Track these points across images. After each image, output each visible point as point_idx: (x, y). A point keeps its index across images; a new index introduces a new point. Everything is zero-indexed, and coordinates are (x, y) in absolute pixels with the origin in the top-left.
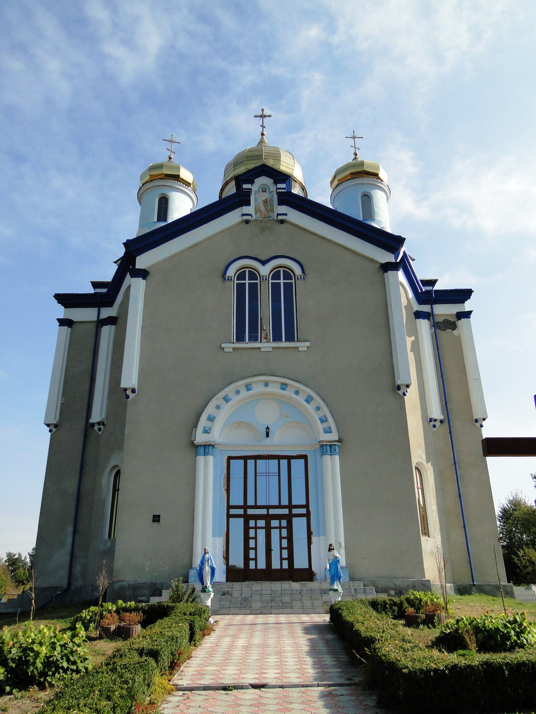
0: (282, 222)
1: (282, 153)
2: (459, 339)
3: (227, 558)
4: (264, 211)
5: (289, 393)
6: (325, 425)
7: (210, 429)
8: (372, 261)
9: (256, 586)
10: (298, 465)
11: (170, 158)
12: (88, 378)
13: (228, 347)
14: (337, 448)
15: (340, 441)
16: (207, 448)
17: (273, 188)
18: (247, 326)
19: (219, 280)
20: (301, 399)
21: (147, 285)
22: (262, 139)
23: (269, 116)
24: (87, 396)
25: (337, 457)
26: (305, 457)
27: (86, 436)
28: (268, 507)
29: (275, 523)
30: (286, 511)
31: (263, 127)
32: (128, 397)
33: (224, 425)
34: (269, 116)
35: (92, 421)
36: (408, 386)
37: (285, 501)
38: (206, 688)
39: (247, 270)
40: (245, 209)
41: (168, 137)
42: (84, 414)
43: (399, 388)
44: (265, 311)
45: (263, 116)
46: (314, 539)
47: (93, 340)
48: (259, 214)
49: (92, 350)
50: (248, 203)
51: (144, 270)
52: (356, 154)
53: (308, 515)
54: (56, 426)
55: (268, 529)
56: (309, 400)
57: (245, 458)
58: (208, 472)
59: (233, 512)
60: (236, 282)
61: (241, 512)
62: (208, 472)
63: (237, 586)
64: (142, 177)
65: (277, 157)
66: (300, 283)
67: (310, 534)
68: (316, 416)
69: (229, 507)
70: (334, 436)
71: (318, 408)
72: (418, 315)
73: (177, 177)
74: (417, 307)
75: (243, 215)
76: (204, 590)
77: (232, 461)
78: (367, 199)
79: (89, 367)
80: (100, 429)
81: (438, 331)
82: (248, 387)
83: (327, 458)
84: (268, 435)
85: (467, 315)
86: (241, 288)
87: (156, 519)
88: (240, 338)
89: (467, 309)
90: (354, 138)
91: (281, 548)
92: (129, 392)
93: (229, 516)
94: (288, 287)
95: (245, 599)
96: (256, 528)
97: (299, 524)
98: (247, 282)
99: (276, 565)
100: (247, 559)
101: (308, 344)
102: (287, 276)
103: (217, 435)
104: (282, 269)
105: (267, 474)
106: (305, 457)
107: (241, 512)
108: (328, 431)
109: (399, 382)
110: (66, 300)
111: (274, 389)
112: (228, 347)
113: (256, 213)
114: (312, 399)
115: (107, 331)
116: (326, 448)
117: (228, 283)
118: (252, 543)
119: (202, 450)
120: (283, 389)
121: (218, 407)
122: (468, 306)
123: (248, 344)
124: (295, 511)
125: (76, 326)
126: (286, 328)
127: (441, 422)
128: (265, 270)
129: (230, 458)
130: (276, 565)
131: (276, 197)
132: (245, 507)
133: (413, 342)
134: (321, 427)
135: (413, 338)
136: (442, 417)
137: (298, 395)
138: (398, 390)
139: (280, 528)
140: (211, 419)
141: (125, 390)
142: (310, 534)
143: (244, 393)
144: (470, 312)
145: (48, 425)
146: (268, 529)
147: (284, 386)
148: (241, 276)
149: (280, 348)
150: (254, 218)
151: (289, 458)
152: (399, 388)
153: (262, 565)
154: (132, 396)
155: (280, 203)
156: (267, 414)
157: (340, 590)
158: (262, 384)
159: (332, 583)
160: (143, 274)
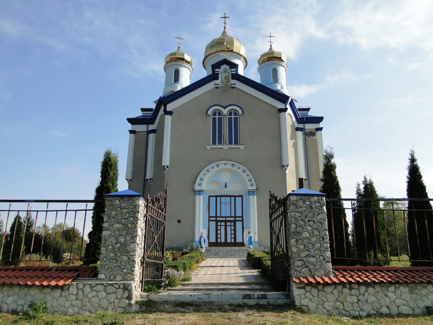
0: (233, 88)
1: (234, 39)
2: (316, 141)
3: (208, 238)
4: (225, 82)
5: (235, 168)
6: (251, 182)
7: (201, 184)
8: (275, 107)
9: (221, 248)
10: (239, 200)
11: (179, 48)
12: (144, 158)
13: (209, 147)
14: (256, 193)
15: (257, 189)
16: (200, 192)
17: (229, 71)
18: (217, 138)
19: (205, 116)
20: (240, 171)
21: (172, 119)
22: (225, 30)
23: (228, 17)
24: (144, 167)
25: (255, 197)
26: (242, 196)
27: (144, 185)
28: (226, 217)
29: (228, 224)
30: (233, 219)
31: (225, 23)
32: (165, 170)
33: (207, 183)
34: (228, 17)
35: (147, 178)
36: (287, 166)
37: (233, 215)
38: (207, 267)
39: (217, 111)
40: (216, 82)
41: (178, 36)
42: (143, 175)
43: (283, 166)
44: (225, 130)
45: (225, 18)
46: (245, 230)
47: (145, 141)
48: (222, 84)
49: (145, 145)
50: (217, 79)
51: (171, 111)
52: (271, 46)
53: (242, 221)
54: (131, 180)
55: (226, 226)
56: (244, 171)
57: (216, 197)
58: (201, 202)
59: (211, 219)
60: (212, 117)
61: (214, 219)
62: (201, 202)
63: (213, 248)
64: (166, 58)
65: (232, 43)
66: (241, 118)
67: (243, 228)
68: (247, 179)
69: (209, 217)
70: (254, 188)
71: (248, 175)
72: (297, 129)
73: (183, 59)
74: (297, 125)
75: (215, 84)
76: (201, 247)
77: (210, 198)
78: (275, 72)
79: (144, 153)
80: (150, 182)
81: (306, 137)
82: (217, 166)
83: (251, 197)
84: (226, 187)
85: (321, 129)
86: (214, 119)
87: (179, 221)
88: (214, 143)
89: (321, 127)
90: (270, 37)
91: (231, 234)
92: (166, 168)
93: (209, 221)
94: (236, 119)
95: (216, 252)
96: (221, 226)
97: (239, 225)
98: (217, 117)
99: (229, 240)
100: (217, 238)
101: (244, 146)
102: (235, 114)
103: (204, 187)
104: (233, 111)
105: (226, 203)
106: (242, 196)
107: (214, 219)
108: (252, 185)
109: (283, 164)
110: (131, 121)
111: (229, 167)
112: (209, 147)
113: (221, 83)
114: (245, 171)
115: (152, 136)
116: (251, 193)
117: (208, 117)
118: (219, 232)
119: (198, 193)
120: (232, 167)
121: (204, 174)
122: (321, 125)
123: (217, 146)
124: (237, 219)
125: (136, 133)
126: (235, 139)
127: (305, 180)
128: (225, 111)
129: (209, 196)
130: (229, 240)
131: (230, 75)
132: (216, 217)
133: (294, 142)
134: (249, 183)
135: (294, 141)
136: (306, 178)
137: (239, 169)
138: (283, 167)
139: (231, 226)
140: (201, 180)
141: (164, 166)
142: (243, 228)
143: (216, 168)
144: (322, 128)
145: (127, 180)
146: (226, 226)
147: (233, 165)
148: (214, 114)
149: (231, 148)
150: (220, 85)
151: (235, 197)
152: (283, 166)
153: (223, 240)
154: (167, 169)
155: (233, 78)
156: (225, 178)
157: (252, 248)
158: (224, 164)
159: (249, 245)
160: (170, 113)
